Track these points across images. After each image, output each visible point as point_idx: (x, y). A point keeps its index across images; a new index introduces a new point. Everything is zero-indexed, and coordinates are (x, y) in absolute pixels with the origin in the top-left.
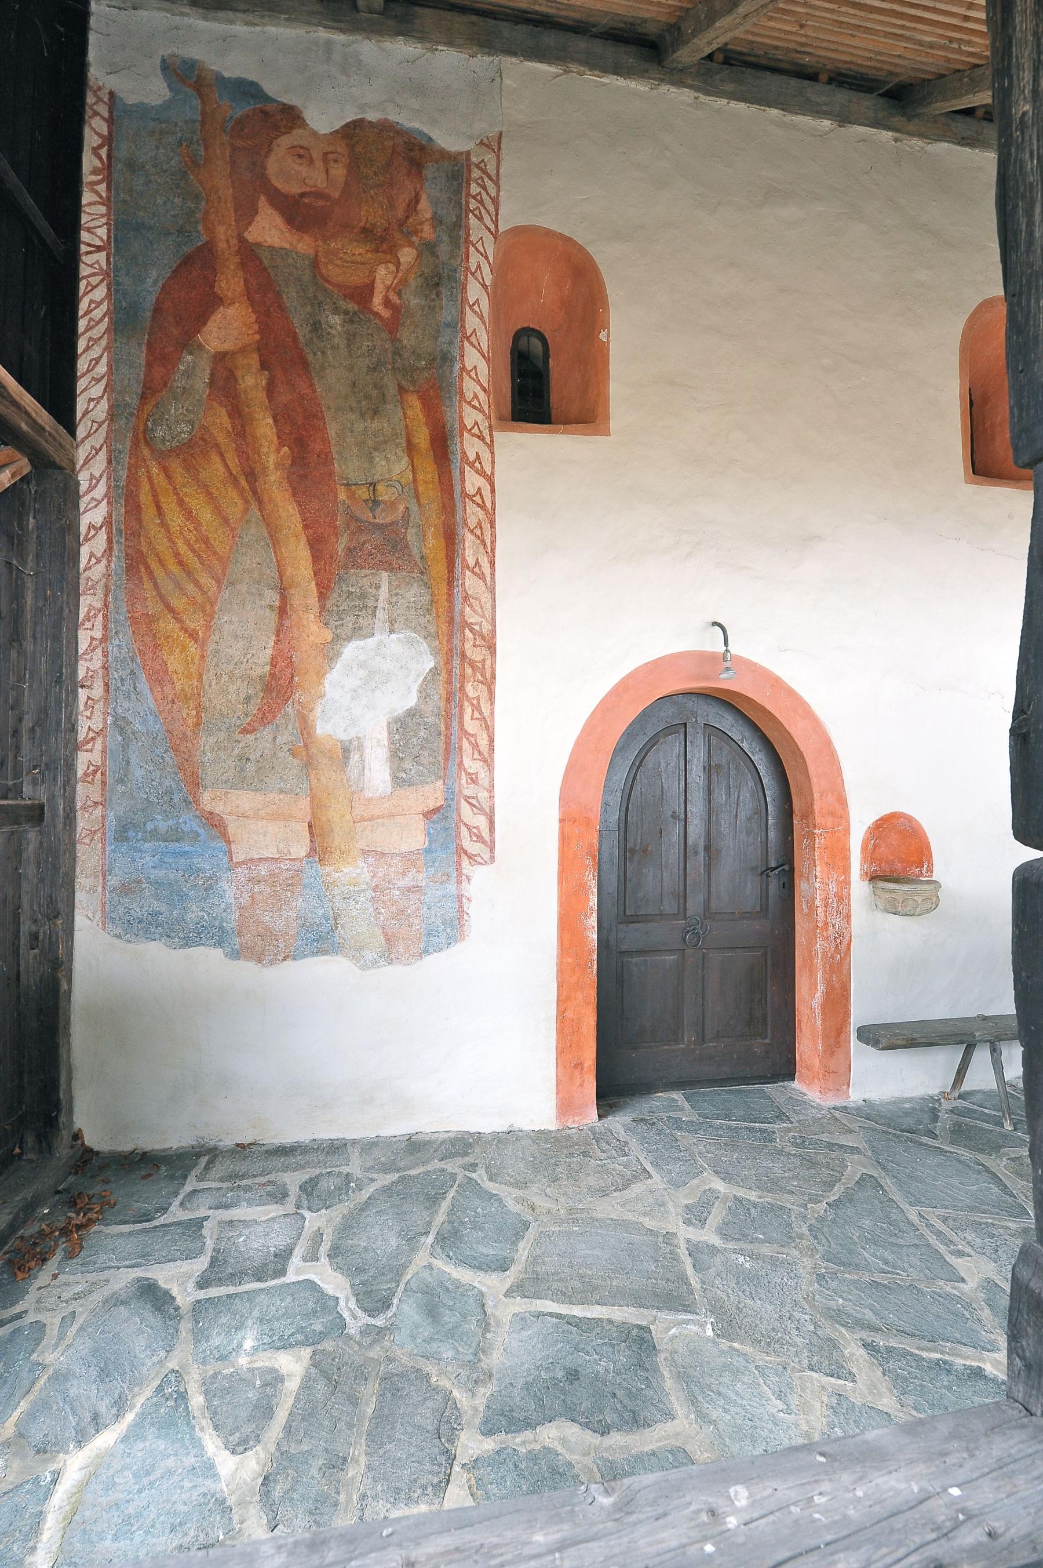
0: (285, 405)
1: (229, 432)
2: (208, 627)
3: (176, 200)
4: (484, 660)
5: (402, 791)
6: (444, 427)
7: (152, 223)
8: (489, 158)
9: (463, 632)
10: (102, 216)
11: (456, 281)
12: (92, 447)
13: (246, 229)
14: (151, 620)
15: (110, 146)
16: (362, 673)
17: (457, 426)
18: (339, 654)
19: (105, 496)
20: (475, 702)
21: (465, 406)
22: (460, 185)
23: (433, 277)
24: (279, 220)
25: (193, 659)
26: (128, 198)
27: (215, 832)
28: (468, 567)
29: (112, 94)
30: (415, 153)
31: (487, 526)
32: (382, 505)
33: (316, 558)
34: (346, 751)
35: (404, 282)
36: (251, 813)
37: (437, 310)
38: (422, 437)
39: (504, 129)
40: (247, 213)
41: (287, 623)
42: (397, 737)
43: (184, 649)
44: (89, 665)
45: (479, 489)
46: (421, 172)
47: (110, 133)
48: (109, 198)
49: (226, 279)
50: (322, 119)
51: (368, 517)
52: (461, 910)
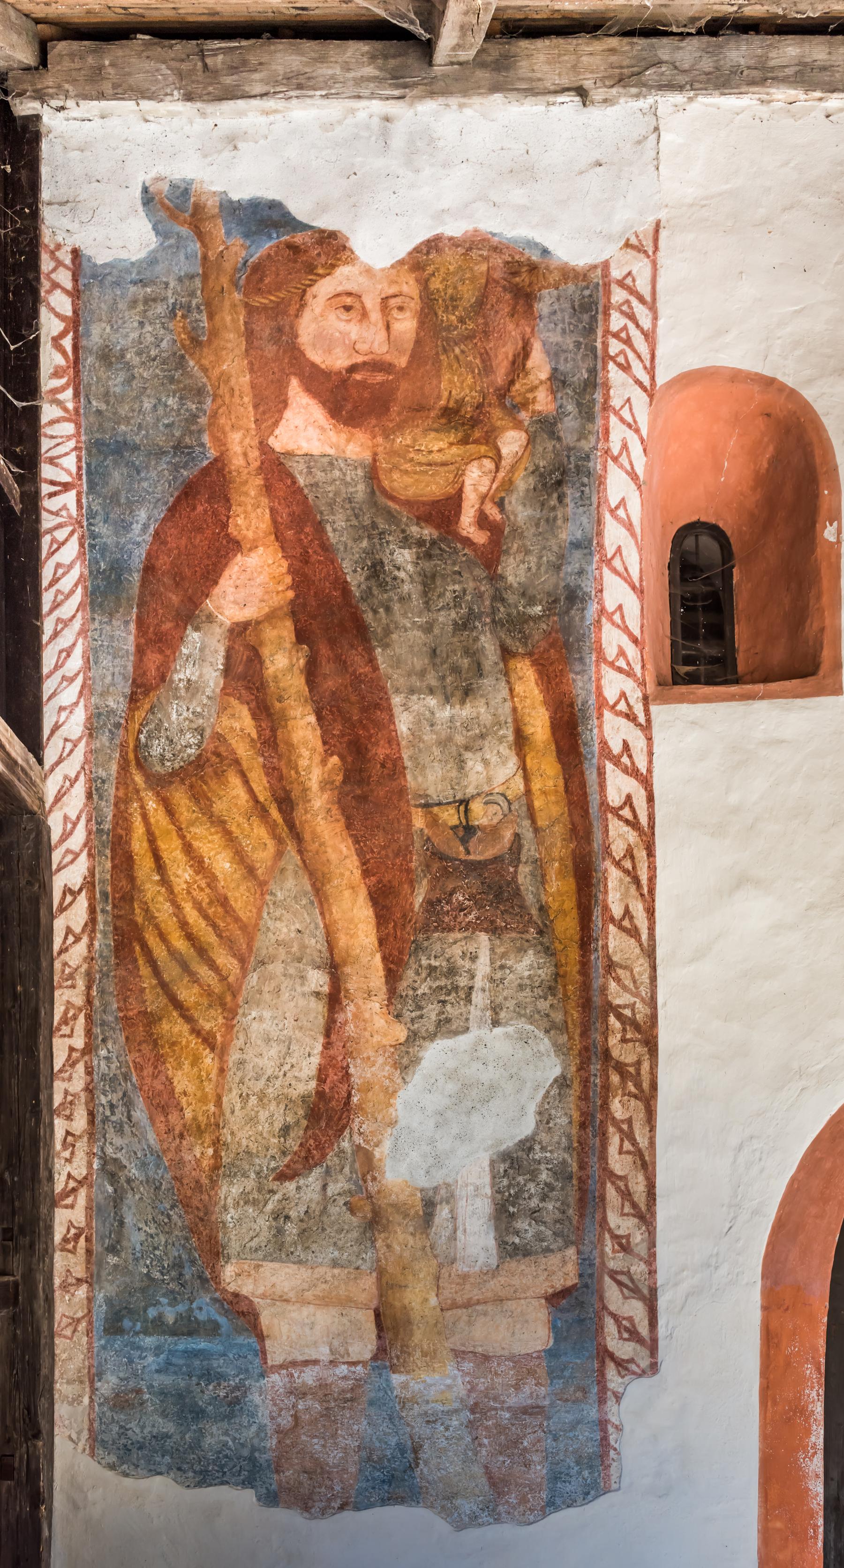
0: (333, 693)
1: (252, 740)
2: (229, 1027)
3: (170, 402)
4: (638, 1063)
5: (514, 1264)
6: (572, 705)
7: (137, 440)
8: (641, 268)
9: (606, 1020)
10: (69, 438)
11: (589, 474)
12: (66, 777)
13: (272, 433)
14: (151, 1020)
15: (76, 332)
16: (451, 1087)
17: (592, 700)
18: (416, 1061)
19: (85, 845)
20: (625, 1127)
21: (605, 669)
22: (594, 319)
23: (552, 472)
24: (318, 413)
25: (208, 1075)
26: (103, 407)
27: (241, 1321)
28: (612, 920)
29: (76, 253)
30: (519, 278)
31: (641, 854)
32: (479, 833)
33: (382, 917)
34: (429, 1205)
35: (508, 485)
36: (292, 1295)
37: (559, 522)
38: (539, 725)
39: (662, 215)
40: (271, 406)
41: (340, 1017)
42: (505, 1182)
43: (196, 1060)
44: (67, 1085)
45: (629, 797)
46: (531, 307)
47: (75, 312)
48: (77, 410)
49: (245, 512)
50: (379, 244)
51: (458, 853)
52: (604, 1441)
